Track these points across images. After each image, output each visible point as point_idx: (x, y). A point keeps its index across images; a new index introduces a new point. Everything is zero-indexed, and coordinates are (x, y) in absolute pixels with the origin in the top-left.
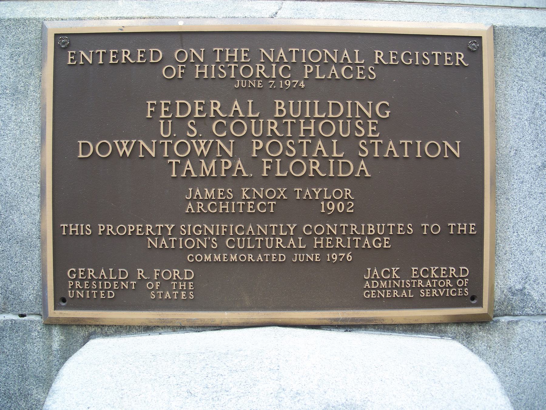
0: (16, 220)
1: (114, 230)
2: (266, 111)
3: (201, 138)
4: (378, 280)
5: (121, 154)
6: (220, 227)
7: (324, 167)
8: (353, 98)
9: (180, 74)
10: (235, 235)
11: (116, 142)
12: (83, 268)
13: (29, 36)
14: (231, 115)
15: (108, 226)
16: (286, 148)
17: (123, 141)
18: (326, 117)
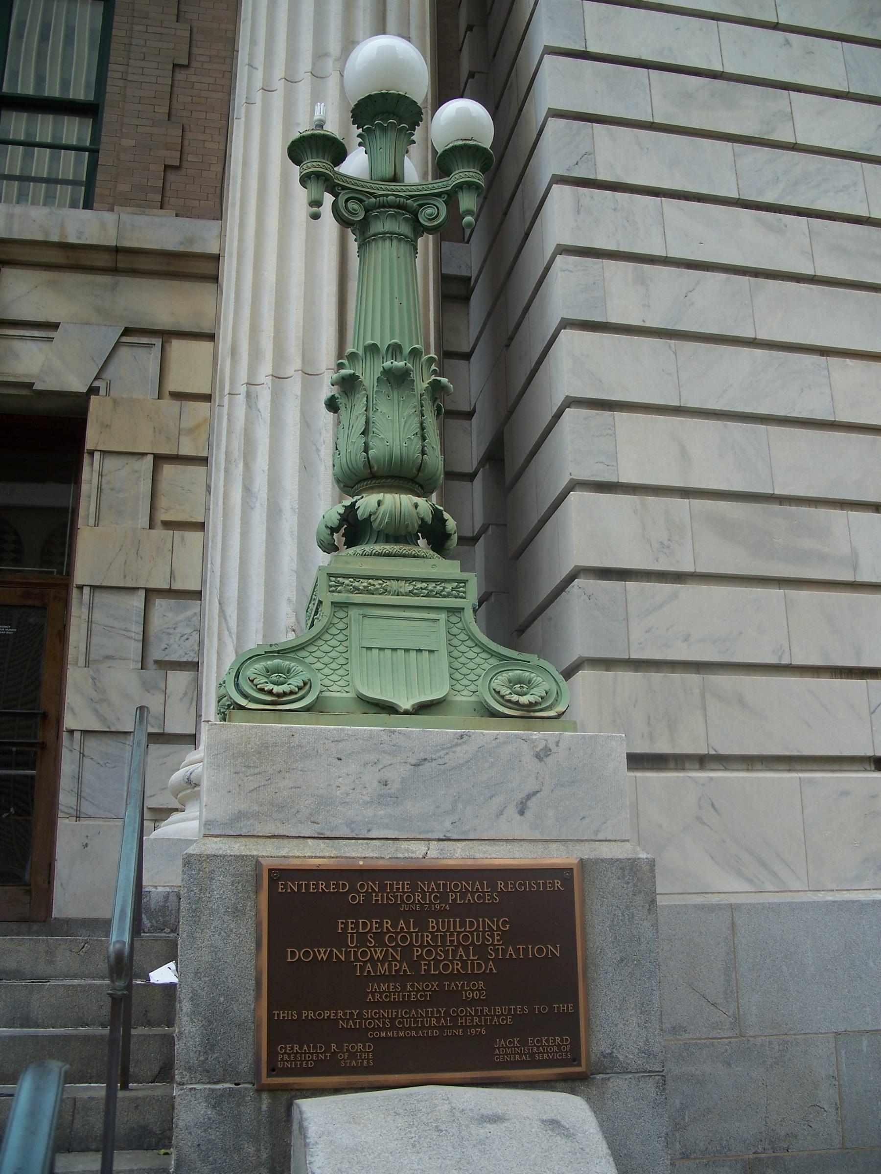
0: (235, 1009)
2: (423, 926)
7: (464, 967)
16: (437, 953)
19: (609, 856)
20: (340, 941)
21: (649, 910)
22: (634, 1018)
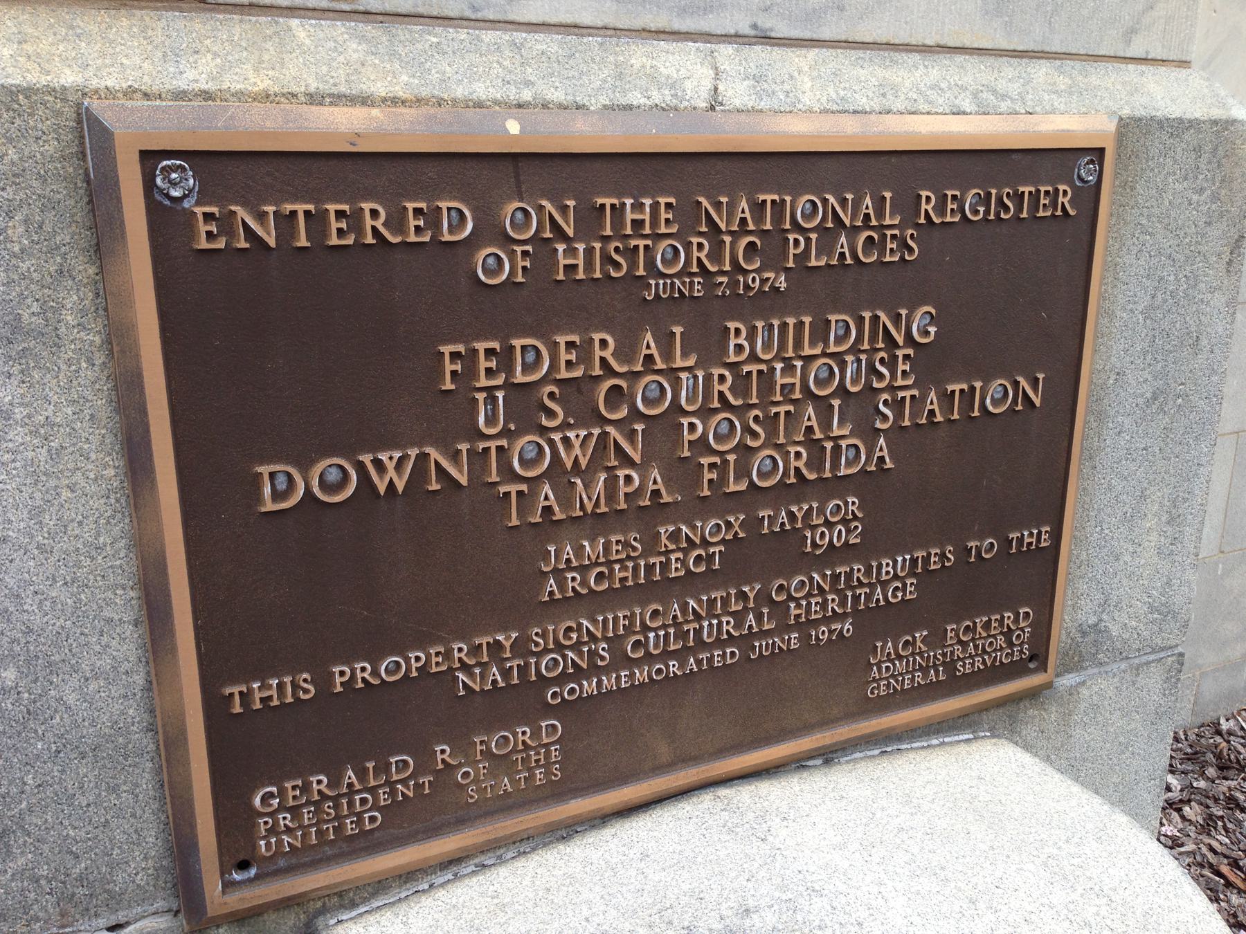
0: (71, 699)
1: (375, 673)
2: (709, 345)
3: (569, 426)
4: (892, 661)
5: (382, 489)
6: (616, 619)
7: (816, 462)
8: (872, 306)
9: (520, 271)
10: (645, 629)
11: (367, 459)
12: (294, 779)
13: (34, 147)
14: (639, 368)
15: (358, 666)
16: (747, 430)
17: (383, 457)
18: (824, 354)
19: (1174, 111)
20: (450, 417)
21: (1230, 263)
22: (1154, 537)
